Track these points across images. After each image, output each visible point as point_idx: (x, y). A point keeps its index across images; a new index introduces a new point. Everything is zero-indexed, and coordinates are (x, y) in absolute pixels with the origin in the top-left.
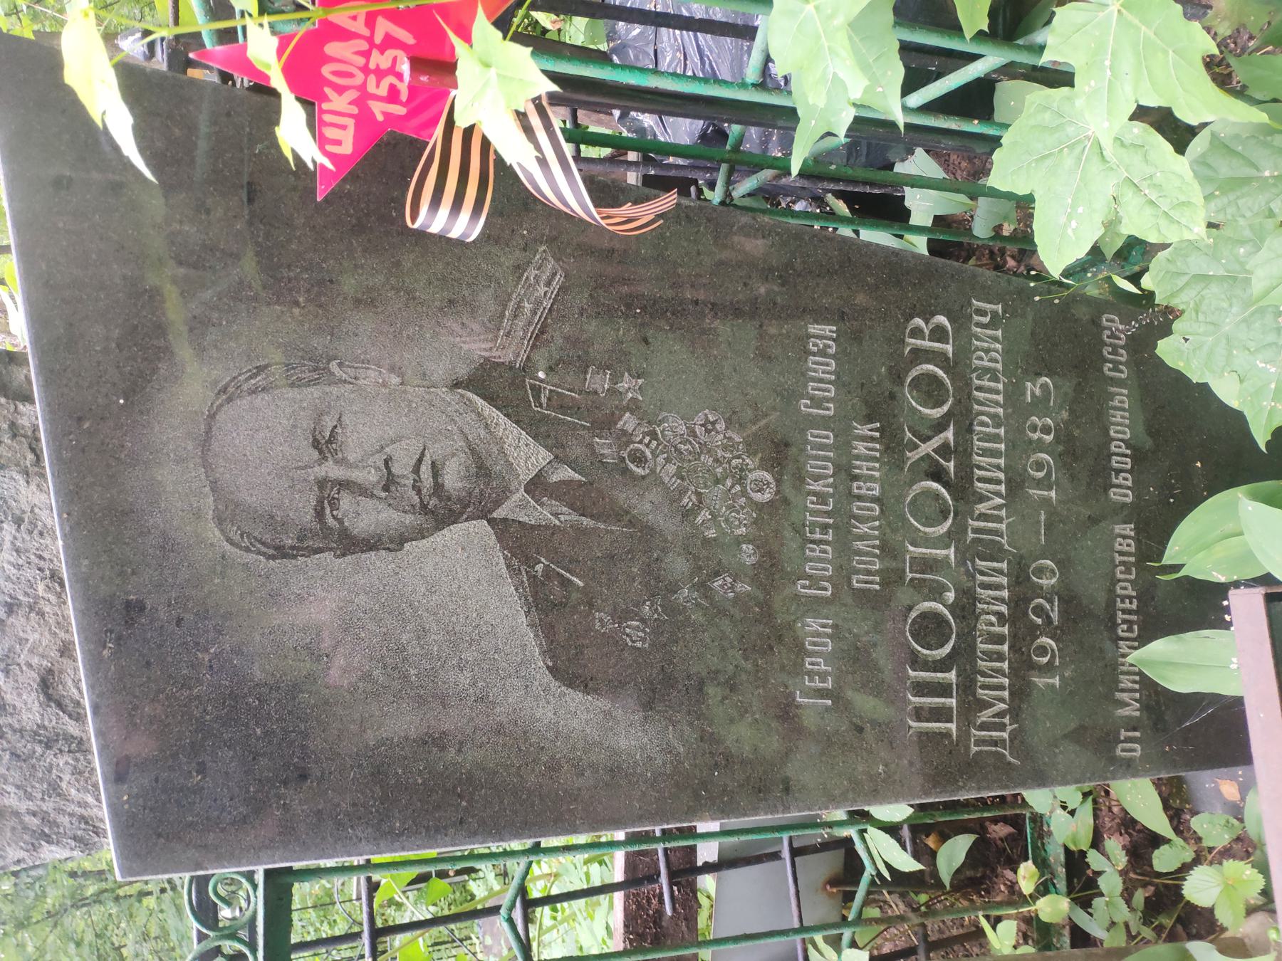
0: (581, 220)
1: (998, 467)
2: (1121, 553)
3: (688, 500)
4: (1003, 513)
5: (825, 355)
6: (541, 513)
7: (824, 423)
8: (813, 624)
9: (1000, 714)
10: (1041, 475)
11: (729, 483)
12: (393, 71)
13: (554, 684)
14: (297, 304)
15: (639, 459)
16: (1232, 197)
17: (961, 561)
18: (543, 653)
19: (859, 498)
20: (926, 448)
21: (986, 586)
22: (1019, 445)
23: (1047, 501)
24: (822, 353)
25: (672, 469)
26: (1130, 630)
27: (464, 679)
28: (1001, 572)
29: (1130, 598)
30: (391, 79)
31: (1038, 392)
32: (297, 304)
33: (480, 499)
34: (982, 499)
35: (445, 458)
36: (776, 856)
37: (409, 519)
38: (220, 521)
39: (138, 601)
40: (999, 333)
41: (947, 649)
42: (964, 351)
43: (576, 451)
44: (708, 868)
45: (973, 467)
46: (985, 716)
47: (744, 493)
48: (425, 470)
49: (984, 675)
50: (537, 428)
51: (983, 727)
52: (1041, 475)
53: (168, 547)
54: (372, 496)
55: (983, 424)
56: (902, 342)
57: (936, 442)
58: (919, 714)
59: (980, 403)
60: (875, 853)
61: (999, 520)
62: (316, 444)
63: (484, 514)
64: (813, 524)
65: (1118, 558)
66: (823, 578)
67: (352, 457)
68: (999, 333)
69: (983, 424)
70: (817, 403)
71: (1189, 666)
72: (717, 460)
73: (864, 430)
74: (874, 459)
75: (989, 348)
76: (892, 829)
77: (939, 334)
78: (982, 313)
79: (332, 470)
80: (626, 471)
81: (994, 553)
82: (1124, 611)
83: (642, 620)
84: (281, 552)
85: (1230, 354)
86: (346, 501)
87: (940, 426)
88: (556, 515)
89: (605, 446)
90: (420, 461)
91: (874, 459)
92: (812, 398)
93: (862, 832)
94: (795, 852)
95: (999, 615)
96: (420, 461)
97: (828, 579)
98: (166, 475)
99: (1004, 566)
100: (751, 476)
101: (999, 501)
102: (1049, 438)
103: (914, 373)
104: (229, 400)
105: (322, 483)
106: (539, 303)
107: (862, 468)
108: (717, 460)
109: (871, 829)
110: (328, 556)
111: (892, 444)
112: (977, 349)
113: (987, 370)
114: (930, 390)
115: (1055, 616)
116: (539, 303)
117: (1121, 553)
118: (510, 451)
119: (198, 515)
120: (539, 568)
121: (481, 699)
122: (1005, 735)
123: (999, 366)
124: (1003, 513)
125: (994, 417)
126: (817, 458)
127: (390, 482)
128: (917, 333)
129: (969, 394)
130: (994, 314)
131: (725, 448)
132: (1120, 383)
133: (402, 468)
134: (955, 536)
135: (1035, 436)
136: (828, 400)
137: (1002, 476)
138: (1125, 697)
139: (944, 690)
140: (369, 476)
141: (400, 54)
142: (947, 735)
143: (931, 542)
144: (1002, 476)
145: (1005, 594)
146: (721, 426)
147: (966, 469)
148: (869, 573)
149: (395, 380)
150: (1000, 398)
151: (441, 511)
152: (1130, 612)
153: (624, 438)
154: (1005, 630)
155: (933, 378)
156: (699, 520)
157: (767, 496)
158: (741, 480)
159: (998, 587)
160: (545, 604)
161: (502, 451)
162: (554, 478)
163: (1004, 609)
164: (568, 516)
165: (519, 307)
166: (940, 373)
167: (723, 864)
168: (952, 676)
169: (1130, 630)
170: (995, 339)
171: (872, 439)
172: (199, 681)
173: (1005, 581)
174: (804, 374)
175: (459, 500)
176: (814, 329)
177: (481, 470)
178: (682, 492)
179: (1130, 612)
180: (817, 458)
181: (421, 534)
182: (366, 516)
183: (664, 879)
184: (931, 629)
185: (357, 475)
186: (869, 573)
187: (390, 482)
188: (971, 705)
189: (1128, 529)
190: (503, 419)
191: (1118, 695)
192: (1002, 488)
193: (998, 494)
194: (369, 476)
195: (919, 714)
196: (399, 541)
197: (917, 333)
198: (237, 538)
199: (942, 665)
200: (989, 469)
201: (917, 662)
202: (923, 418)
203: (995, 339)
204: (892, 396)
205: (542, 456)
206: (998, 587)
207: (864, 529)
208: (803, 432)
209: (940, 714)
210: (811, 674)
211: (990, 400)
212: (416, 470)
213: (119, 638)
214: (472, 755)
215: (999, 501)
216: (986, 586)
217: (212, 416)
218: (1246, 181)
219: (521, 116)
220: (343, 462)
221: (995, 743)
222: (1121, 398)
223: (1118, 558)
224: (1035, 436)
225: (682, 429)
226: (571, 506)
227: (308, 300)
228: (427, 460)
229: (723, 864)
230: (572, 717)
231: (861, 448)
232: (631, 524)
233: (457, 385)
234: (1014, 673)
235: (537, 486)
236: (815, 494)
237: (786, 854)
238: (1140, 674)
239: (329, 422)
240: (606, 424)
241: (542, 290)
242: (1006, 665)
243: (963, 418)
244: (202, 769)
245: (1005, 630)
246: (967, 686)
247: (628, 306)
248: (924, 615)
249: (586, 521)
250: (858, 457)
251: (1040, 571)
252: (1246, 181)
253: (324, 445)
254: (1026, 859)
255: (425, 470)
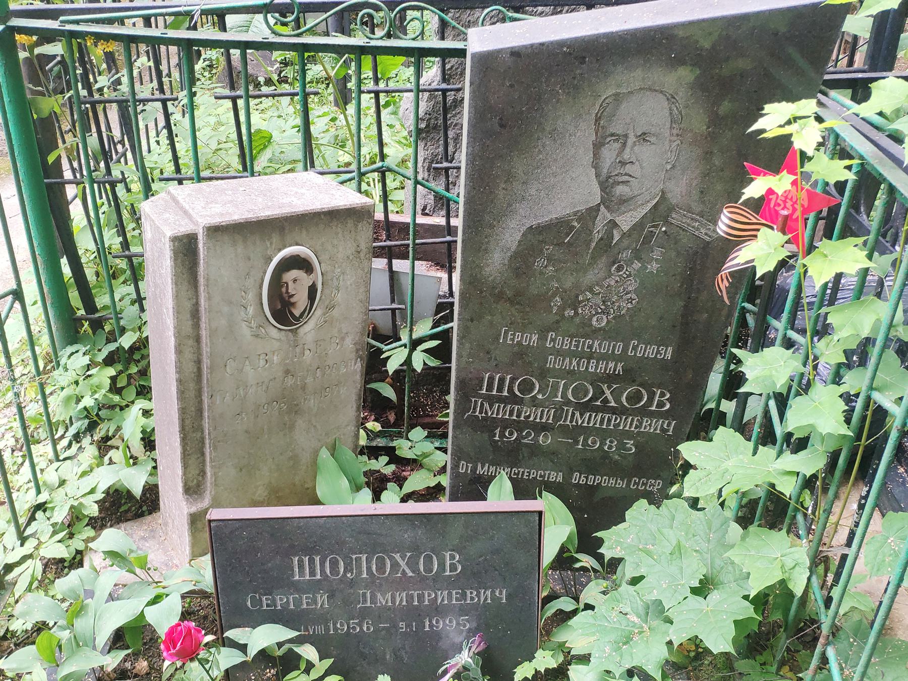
0: (724, 264)
1: (595, 424)
2: (549, 474)
3: (597, 289)
4: (574, 423)
5: (657, 354)
6: (600, 225)
7: (625, 349)
8: (535, 338)
9: (486, 413)
10: (590, 442)
11: (603, 307)
12: (785, 208)
13: (525, 228)
14: (708, 128)
15: (619, 269)
16: (704, 523)
17: (554, 403)
18: (539, 224)
19: (588, 363)
20: (608, 393)
21: (542, 412)
22: (603, 434)
23: (577, 443)
24: (658, 352)
25: (612, 283)
26: (515, 474)
27: (533, 192)
28: (548, 419)
29: (529, 476)
30: (782, 206)
31: (628, 446)
32: (708, 128)
33: (608, 200)
34: (581, 415)
35: (630, 186)
36: (393, 301)
37: (605, 171)
38: (617, 95)
39: (585, 62)
40: (658, 432)
41: (518, 393)
42: (652, 414)
43: (626, 242)
44: (390, 265)
45: (597, 413)
46: (486, 405)
47: (597, 313)
48: (626, 178)
49: (504, 407)
50: (638, 227)
51: (482, 404)
52: (590, 442)
53: (607, 74)
54: (617, 156)
55: (616, 419)
56: (659, 388)
57: (610, 398)
58: (491, 379)
59: (626, 419)
60: (395, 351)
61: (571, 422)
62: (644, 134)
63: (603, 201)
64: (579, 341)
65: (547, 473)
66: (555, 343)
67: (636, 148)
68: (658, 432)
69: (616, 419)
70: (635, 348)
71: (500, 495)
72: (614, 302)
73: (620, 367)
74: (606, 369)
75: (651, 426)
76: (408, 361)
77: (661, 405)
78: (669, 425)
79: (630, 142)
80: (614, 263)
81: (557, 418)
82: (523, 472)
83: (546, 267)
84: (598, 119)
85: (636, 526)
86: (617, 146)
87: (618, 400)
88: (598, 232)
89: (627, 254)
90: (630, 176)
91: (606, 369)
92: (637, 346)
93: (405, 346)
94: (393, 311)
95: (529, 416)
96: (630, 176)
97: (554, 346)
98: (639, 73)
99: (550, 421)
100: (604, 317)
101: (580, 422)
102: (606, 448)
103: (643, 391)
104: (668, 99)
105: (626, 136)
106: (698, 229)
107: (602, 365)
108: (614, 302)
109: (407, 351)
110: (594, 138)
111: (610, 378)
112: (652, 421)
113: (641, 424)
114: (635, 397)
115: (525, 441)
116: (698, 229)
117: (549, 474)
118: (630, 213)
119: (619, 86)
120: (576, 224)
121: (523, 198)
122: (477, 414)
123: (642, 430)
124: (574, 423)
125: (619, 424)
126: (609, 346)
127: (623, 163)
128: (662, 395)
129: (631, 415)
130: (668, 430)
131: (619, 307)
132: (628, 484)
133: (628, 169)
134: (568, 403)
135: (608, 442)
136: (635, 354)
137: (591, 425)
138: (486, 468)
139: (500, 389)
140: (626, 156)
141: (790, 212)
142: (481, 389)
143: (564, 391)
144: (591, 425)
145: (538, 420)
146: (629, 306)
147: (597, 410)
148: (555, 363)
149: (669, 167)
150: (627, 428)
151: (606, 185)
152: (523, 475)
153: (629, 263)
154: (522, 418)
155: (640, 400)
156: (588, 293)
157: (594, 323)
158: (603, 312)
159: (541, 418)
160: (560, 227)
161: (631, 210)
162: (615, 232)
163: (531, 419)
164: (597, 237)
165: (696, 221)
166: (642, 403)
167: (393, 276)
168: (505, 393)
169: (515, 474)
170: (655, 430)
171: (615, 370)
172: (548, 86)
173: (544, 421)
174: (649, 343)
175: (611, 192)
176: (670, 349)
177: (623, 201)
178: (601, 287)
179: (523, 475)
180: (609, 346)
181: (597, 175)
182: (609, 154)
183: (389, 243)
184: (527, 387)
185: (628, 150)
186: (555, 363)
187: (623, 163)
188: (491, 400)
189: (560, 479)
190: (645, 212)
191: (487, 465)
192: (585, 424)
193: (583, 422)
194: (626, 156)
195: (491, 379)
196: (596, 166)
197: (662, 395)
198: (607, 101)
199: (510, 390)
200: (594, 420)
201: (513, 380)
202: (622, 393)
203: (655, 430)
204: (634, 381)
205: (625, 227)
206: (541, 418)
207: (574, 363)
208: (622, 341)
209: (490, 388)
210: (514, 335)
211: (627, 424)
212: (626, 174)
213: (570, 54)
214: (501, 194)
215: (580, 422)
216: (542, 412)
217: (661, 92)
218: (710, 529)
219: (753, 261)
220: (634, 144)
221: (475, 409)
222: (621, 484)
223: (547, 473)
224: (608, 442)
225: (630, 288)
226: (601, 239)
227: (709, 132)
228: (632, 179)
229: (393, 276)
230: (510, 235)
231: (611, 365)
232: (589, 264)
233: (663, 192)
234: (503, 420)
235: (613, 224)
236: (593, 343)
237: (394, 306)
238: (495, 476)
239: (653, 139)
240: (637, 255)
241: (703, 231)
242: (507, 417)
243: (620, 411)
244: (511, 86)
245: (522, 418)
246: (501, 400)
247: (690, 269)
248: (533, 384)
249: (593, 244)
250: (607, 363)
251: (546, 436)
252: (710, 529)
253: (643, 137)
254: (382, 427)
255: (626, 178)
